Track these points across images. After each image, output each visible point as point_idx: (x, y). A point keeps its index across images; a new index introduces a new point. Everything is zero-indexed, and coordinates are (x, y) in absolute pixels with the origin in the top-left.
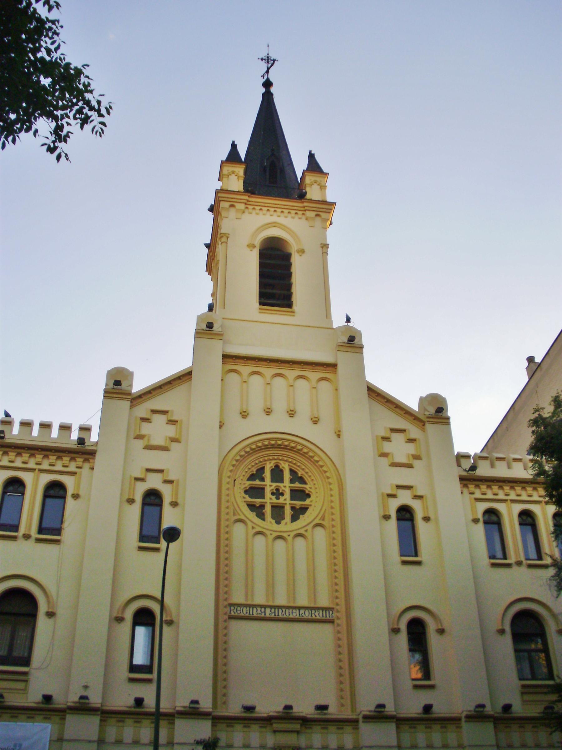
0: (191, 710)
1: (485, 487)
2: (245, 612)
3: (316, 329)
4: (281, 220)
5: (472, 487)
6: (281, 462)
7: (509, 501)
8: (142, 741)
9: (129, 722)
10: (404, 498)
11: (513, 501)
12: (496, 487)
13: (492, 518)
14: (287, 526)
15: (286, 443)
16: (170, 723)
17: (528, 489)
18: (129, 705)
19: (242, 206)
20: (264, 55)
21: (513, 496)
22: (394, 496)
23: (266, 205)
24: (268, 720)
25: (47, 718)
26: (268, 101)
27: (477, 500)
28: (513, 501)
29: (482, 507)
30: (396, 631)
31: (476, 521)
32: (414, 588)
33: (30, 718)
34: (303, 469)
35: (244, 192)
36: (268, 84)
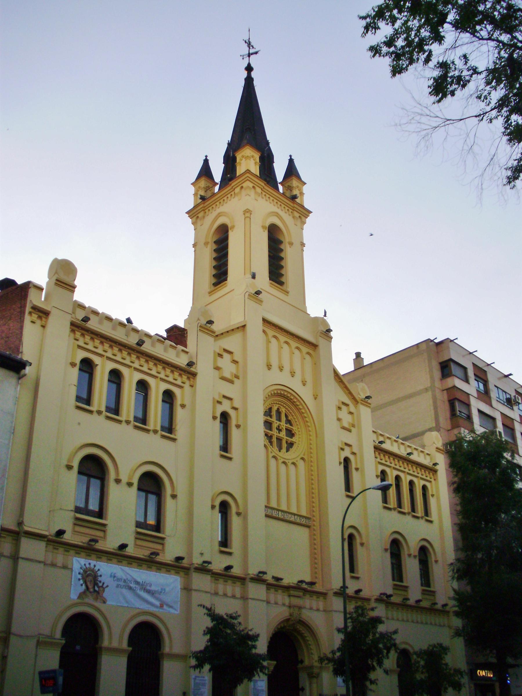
0: (89, 546)
1: (161, 367)
2: (280, 515)
3: (291, 307)
4: (282, 213)
5: (78, 334)
6: (281, 407)
7: (105, 357)
8: (237, 596)
9: (221, 581)
10: (226, 406)
11: (109, 358)
12: (161, 367)
13: (87, 366)
14: (283, 454)
15: (292, 397)
16: (185, 574)
17: (141, 359)
18: (116, 548)
19: (259, 190)
20: (246, 39)
21: (136, 365)
22: (219, 403)
23: (254, 182)
24: (287, 588)
25: (177, 573)
26: (249, 82)
27: (79, 347)
28: (109, 358)
29: (82, 355)
30: (213, 507)
31: (73, 365)
32: (226, 477)
33: (168, 571)
34: (292, 416)
35: (290, 199)
36: (249, 69)
